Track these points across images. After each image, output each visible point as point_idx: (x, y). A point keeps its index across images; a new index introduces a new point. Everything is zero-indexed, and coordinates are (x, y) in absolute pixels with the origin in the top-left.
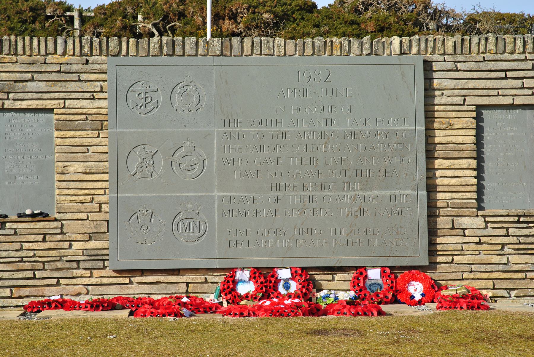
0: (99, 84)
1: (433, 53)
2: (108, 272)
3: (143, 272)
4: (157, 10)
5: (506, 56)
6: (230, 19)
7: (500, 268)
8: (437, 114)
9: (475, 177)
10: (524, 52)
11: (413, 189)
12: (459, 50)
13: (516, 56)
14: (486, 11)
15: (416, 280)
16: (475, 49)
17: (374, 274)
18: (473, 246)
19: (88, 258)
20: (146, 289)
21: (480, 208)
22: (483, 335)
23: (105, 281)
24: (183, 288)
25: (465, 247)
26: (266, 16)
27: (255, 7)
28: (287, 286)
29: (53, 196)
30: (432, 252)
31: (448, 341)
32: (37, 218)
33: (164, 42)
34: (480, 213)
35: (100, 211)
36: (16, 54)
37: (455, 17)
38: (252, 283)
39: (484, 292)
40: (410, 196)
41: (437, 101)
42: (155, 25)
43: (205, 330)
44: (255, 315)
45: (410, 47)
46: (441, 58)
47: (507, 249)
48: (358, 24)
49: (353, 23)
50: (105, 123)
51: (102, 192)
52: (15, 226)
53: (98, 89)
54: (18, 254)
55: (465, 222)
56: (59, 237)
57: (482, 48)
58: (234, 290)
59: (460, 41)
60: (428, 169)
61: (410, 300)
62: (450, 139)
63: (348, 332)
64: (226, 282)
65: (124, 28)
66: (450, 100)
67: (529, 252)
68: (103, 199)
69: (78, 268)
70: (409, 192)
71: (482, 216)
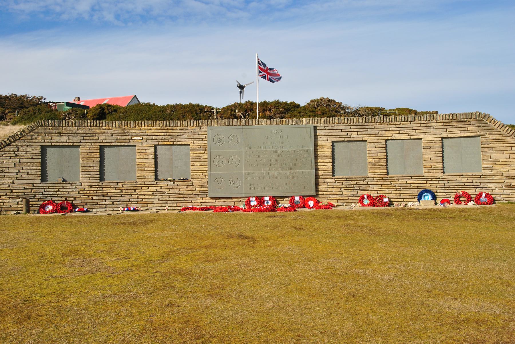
0: (204, 135)
1: (317, 123)
2: (208, 198)
3: (219, 198)
4: (243, 108)
5: (342, 124)
6: (268, 111)
7: (340, 196)
8: (318, 144)
9: (332, 165)
10: (348, 123)
11: (310, 170)
12: (326, 123)
13: (345, 125)
14: (362, 107)
15: (311, 200)
16: (331, 122)
17: (297, 198)
18: (331, 189)
19: (201, 193)
20: (220, 204)
21: (333, 176)
22: (325, 217)
23: (207, 201)
24: (233, 204)
25: (328, 189)
26: (281, 109)
27: (277, 107)
28: (267, 203)
29: (190, 173)
30: (317, 190)
31: (313, 219)
32: (185, 180)
33: (226, 121)
34: (333, 177)
35: (205, 178)
36: (178, 127)
37: (351, 109)
38: (256, 202)
39: (334, 204)
40: (309, 172)
41: (318, 140)
42: (242, 114)
43: (235, 216)
44: (253, 212)
45: (309, 121)
46: (320, 125)
47: (342, 189)
48: (315, 112)
49: (313, 111)
50: (207, 149)
51: (206, 171)
52: (178, 183)
53: (204, 137)
54: (179, 192)
55: (328, 180)
56: (192, 187)
57: (333, 122)
58: (250, 204)
59: (326, 119)
60: (315, 163)
61: (309, 207)
62: (323, 152)
63: (281, 217)
64: (247, 202)
65: (231, 115)
66: (323, 139)
67: (350, 190)
68: (206, 174)
69: (198, 197)
70: (309, 170)
71: (334, 178)
